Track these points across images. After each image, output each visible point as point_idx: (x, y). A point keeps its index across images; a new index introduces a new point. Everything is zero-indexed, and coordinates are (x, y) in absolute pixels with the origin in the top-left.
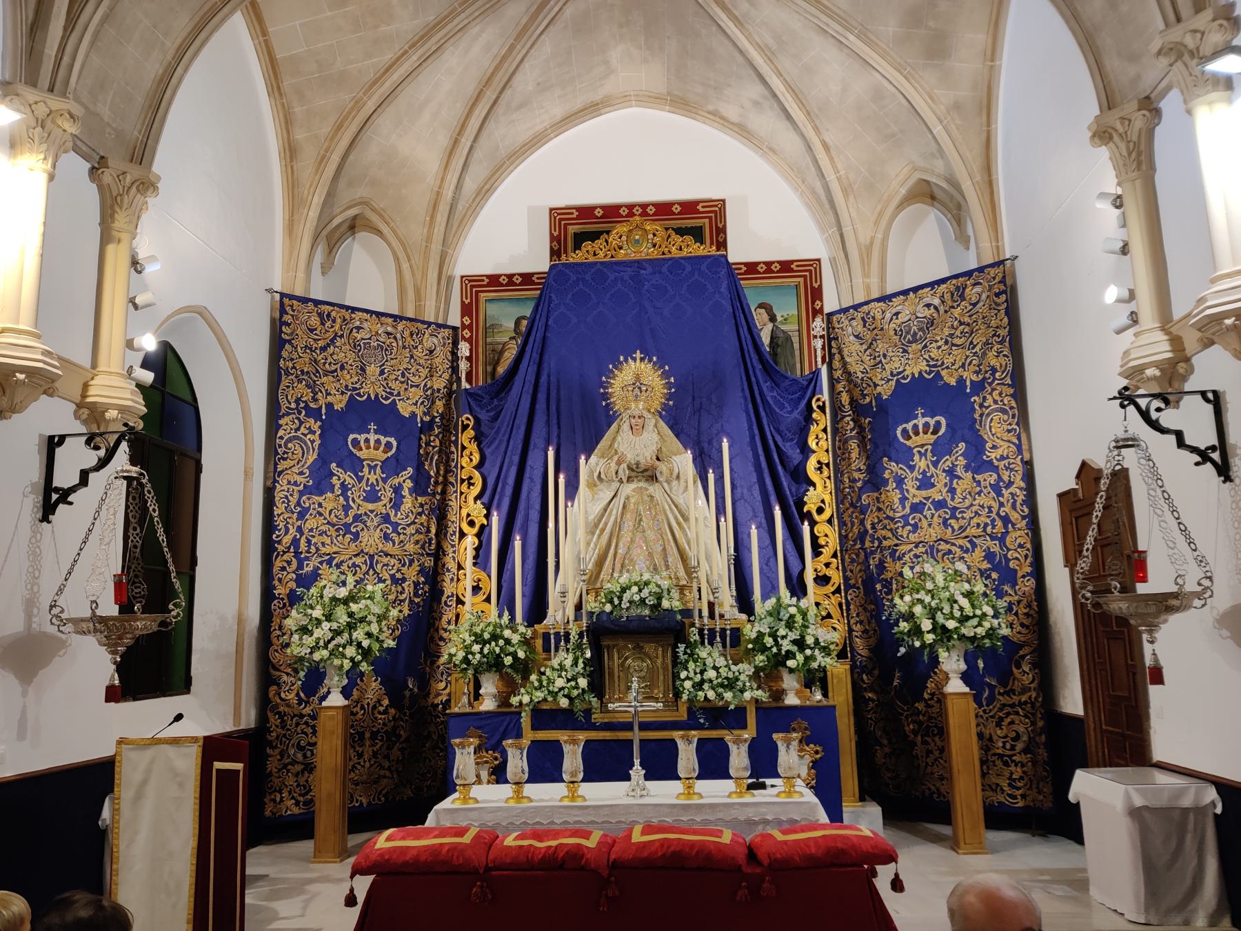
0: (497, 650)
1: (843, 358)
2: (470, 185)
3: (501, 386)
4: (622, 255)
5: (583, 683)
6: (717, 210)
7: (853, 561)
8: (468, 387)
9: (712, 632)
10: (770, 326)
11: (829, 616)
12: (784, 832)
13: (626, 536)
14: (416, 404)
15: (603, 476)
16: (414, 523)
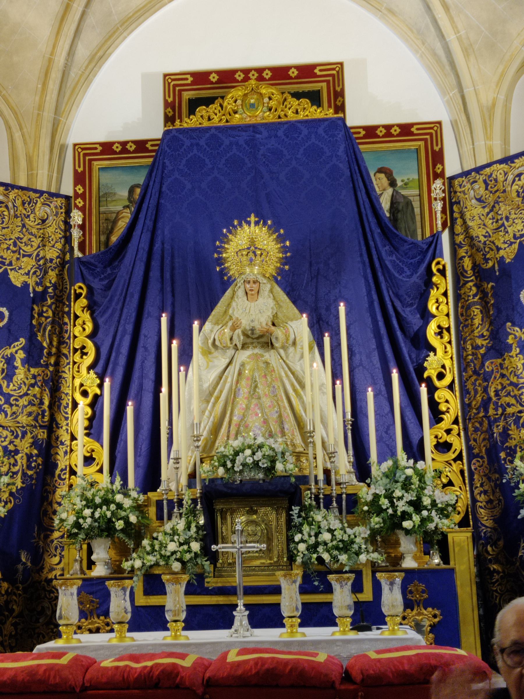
0: (109, 514)
1: (465, 222)
2: (82, 52)
3: (115, 254)
4: (236, 120)
5: (196, 546)
6: (335, 74)
7: (476, 430)
8: (80, 255)
9: (328, 500)
10: (390, 191)
11: (450, 483)
12: (378, 652)
13: (242, 402)
14: (28, 274)
15: (217, 343)
16: (26, 394)
